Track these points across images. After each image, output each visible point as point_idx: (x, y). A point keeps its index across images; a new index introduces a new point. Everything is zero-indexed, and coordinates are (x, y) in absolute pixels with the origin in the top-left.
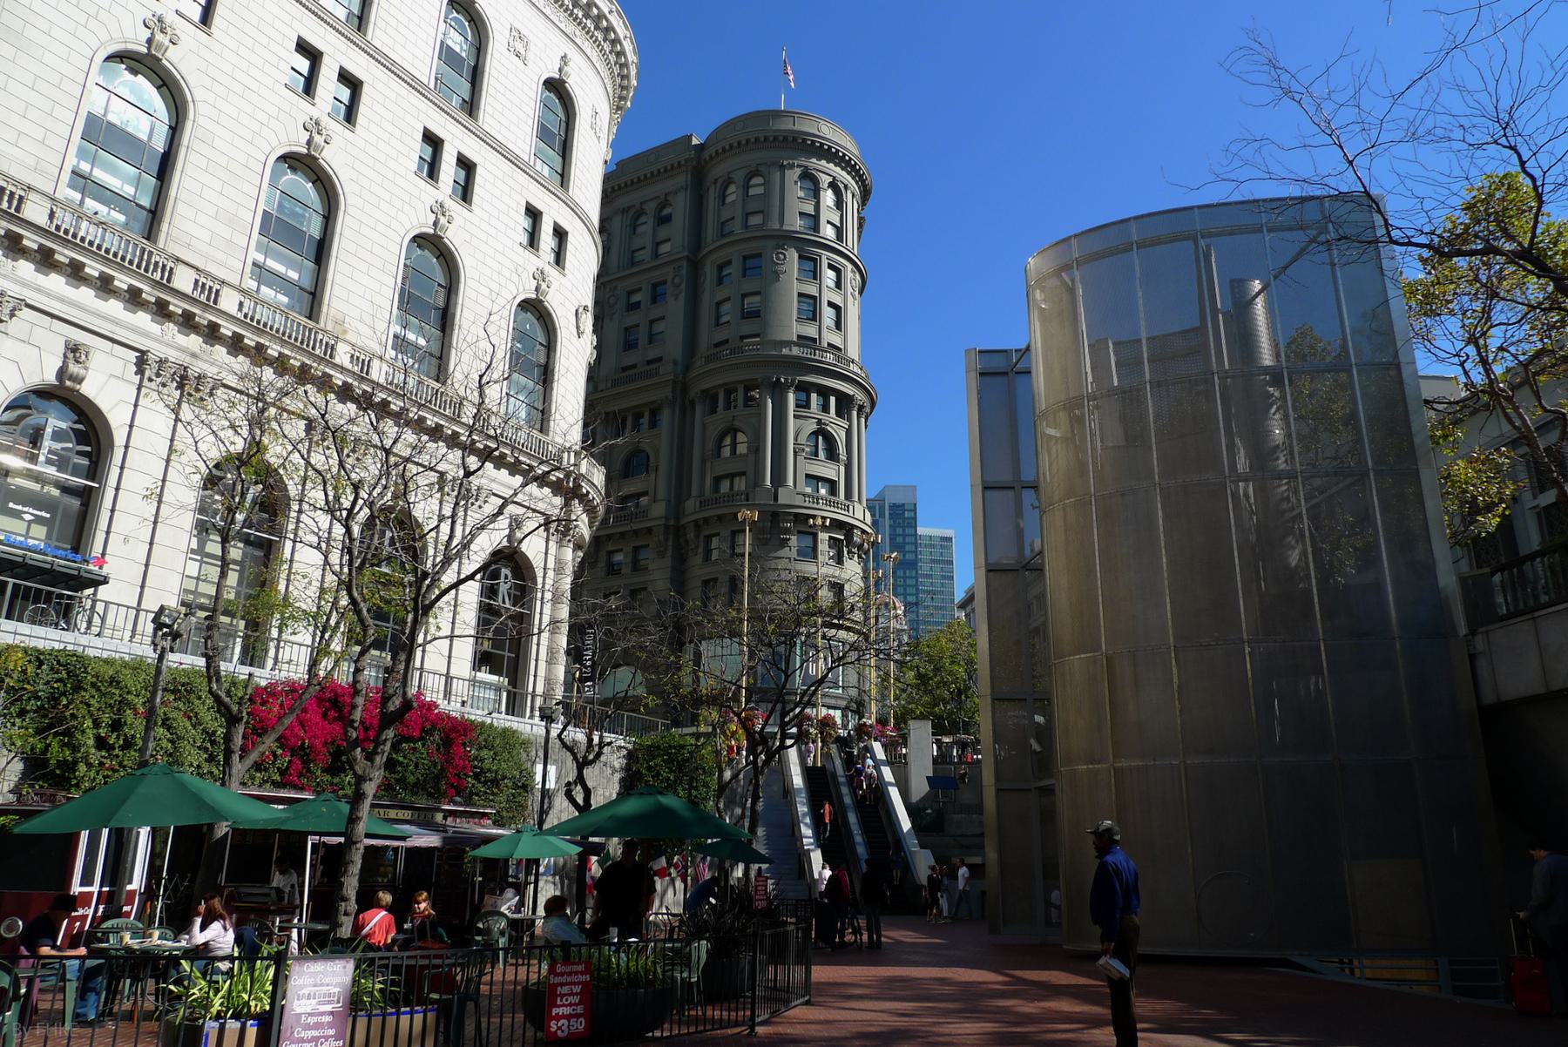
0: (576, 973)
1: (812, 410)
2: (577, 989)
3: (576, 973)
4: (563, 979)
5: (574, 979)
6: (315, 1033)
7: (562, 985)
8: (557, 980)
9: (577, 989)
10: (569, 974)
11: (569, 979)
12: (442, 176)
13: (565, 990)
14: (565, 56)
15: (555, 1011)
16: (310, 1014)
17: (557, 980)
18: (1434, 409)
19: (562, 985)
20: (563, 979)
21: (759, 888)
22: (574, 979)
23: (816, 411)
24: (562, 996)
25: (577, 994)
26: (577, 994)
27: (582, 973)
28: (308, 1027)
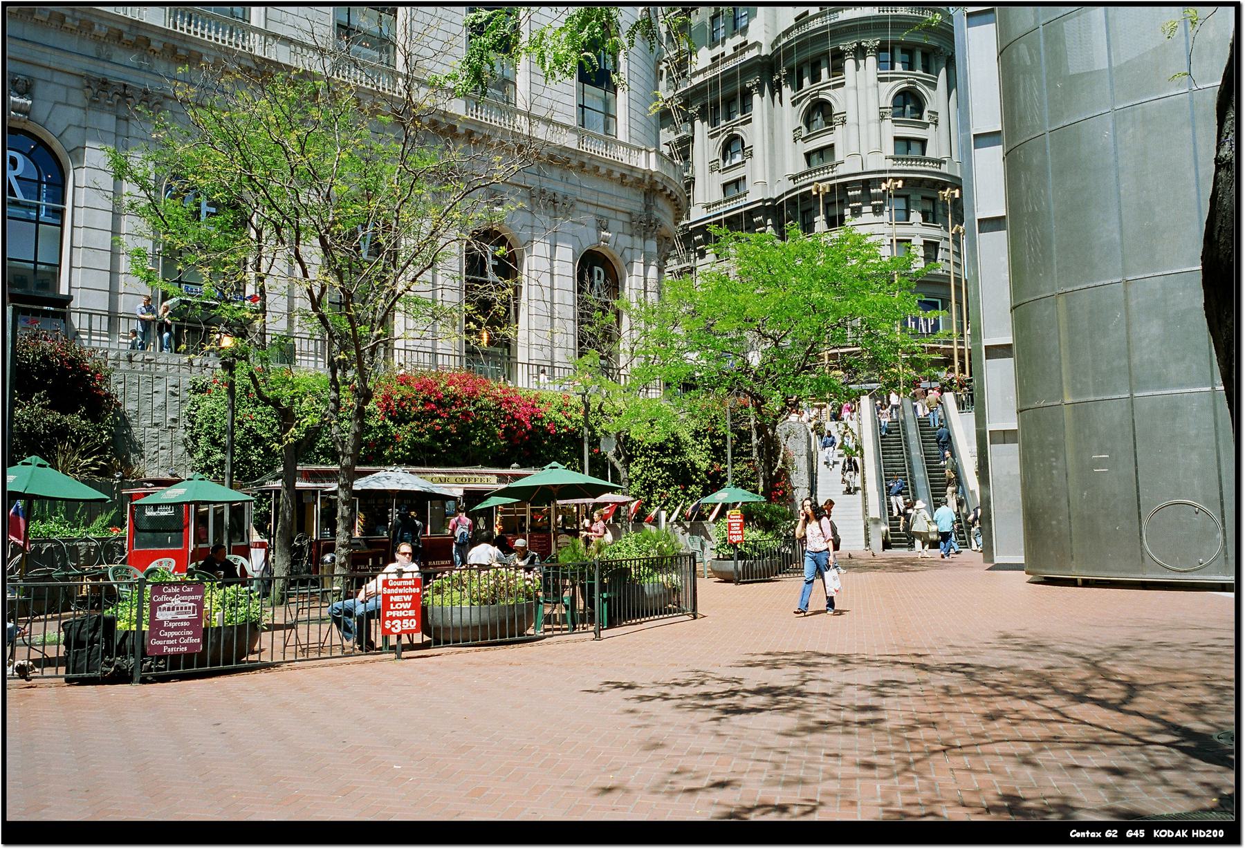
0: (407, 587)
1: (896, 71)
2: (409, 598)
3: (407, 587)
4: (396, 591)
5: (405, 590)
6: (177, 634)
7: (394, 595)
8: (389, 591)
9: (409, 598)
10: (401, 587)
11: (401, 591)
12: (927, 678)
13: (397, 599)
14: (580, 356)
15: (388, 614)
16: (170, 621)
17: (389, 591)
18: (1165, 782)
19: (394, 595)
20: (396, 591)
21: (562, 375)
22: (405, 590)
23: (901, 71)
24: (395, 603)
25: (408, 602)
26: (408, 602)
27: (412, 587)
28: (169, 629)
